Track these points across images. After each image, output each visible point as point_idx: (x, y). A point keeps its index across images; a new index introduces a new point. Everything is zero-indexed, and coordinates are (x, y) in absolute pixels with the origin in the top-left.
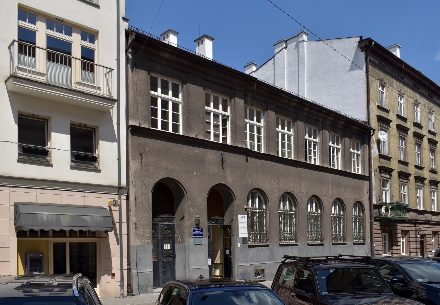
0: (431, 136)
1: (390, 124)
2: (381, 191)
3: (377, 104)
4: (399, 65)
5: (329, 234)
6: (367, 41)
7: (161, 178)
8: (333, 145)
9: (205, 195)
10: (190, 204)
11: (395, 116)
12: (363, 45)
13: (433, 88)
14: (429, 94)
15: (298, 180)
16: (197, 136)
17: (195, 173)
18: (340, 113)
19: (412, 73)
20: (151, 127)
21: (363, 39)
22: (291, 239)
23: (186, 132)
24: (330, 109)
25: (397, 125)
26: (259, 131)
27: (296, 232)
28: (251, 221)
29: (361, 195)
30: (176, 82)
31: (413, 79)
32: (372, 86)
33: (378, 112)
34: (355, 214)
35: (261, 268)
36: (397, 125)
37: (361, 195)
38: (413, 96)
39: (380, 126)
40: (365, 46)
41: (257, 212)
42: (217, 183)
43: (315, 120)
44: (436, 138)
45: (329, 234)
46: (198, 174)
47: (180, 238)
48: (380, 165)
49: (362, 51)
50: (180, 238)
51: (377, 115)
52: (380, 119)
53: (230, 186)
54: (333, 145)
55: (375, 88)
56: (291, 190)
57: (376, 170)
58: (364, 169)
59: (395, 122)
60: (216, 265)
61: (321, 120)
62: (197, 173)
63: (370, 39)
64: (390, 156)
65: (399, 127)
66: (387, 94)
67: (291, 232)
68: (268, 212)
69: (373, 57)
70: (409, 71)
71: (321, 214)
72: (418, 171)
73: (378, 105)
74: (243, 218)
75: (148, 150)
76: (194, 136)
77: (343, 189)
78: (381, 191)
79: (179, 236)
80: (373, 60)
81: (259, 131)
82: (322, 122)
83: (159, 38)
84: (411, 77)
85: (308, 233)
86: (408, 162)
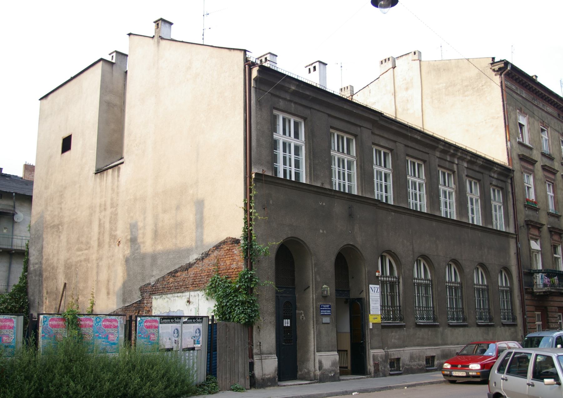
0: (547, 162)
1: (535, 165)
2: (530, 254)
3: (518, 140)
4: (540, 90)
5: (472, 312)
6: (502, 64)
7: (285, 237)
8: (342, 156)
9: (333, 258)
10: (317, 270)
11: (540, 155)
12: (496, 68)
13: (560, 103)
14: (559, 115)
15: (434, 239)
16: (322, 184)
17: (321, 231)
18: (457, 144)
19: (556, 100)
20: (256, 171)
21: (496, 60)
22: (428, 319)
23: (310, 179)
24: (443, 139)
25: (542, 166)
26: (297, 152)
27: (433, 307)
28: (425, 295)
29: (508, 259)
30: (298, 120)
31: (557, 107)
32: (510, 118)
33: (520, 149)
34: (450, 280)
35: (396, 357)
36: (542, 166)
37: (508, 259)
38: (558, 129)
39: (523, 167)
40: (500, 69)
41: (429, 285)
42: (346, 243)
43: (449, 162)
44: (556, 165)
45: (472, 312)
46: (325, 232)
47: (303, 315)
48: (526, 219)
49: (496, 75)
50: (303, 315)
51: (519, 154)
52: (523, 158)
53: (359, 248)
54: (342, 156)
55: (514, 120)
56: (426, 253)
57: (523, 226)
58: (507, 224)
59: (541, 161)
60: (342, 352)
61: (456, 162)
62: (323, 231)
63: (505, 61)
64: (538, 207)
65: (544, 168)
66: (529, 127)
67: (394, 307)
68: (401, 281)
69: (509, 82)
70: (525, 80)
71: (461, 284)
72: (530, 213)
73: (518, 141)
74: (376, 291)
75: (271, 202)
76: (319, 185)
77: (486, 250)
78: (530, 254)
79: (302, 313)
80: (509, 85)
81: (297, 152)
82: (457, 164)
83: (317, 85)
84: (554, 105)
85: (416, 308)
86: (559, 214)
